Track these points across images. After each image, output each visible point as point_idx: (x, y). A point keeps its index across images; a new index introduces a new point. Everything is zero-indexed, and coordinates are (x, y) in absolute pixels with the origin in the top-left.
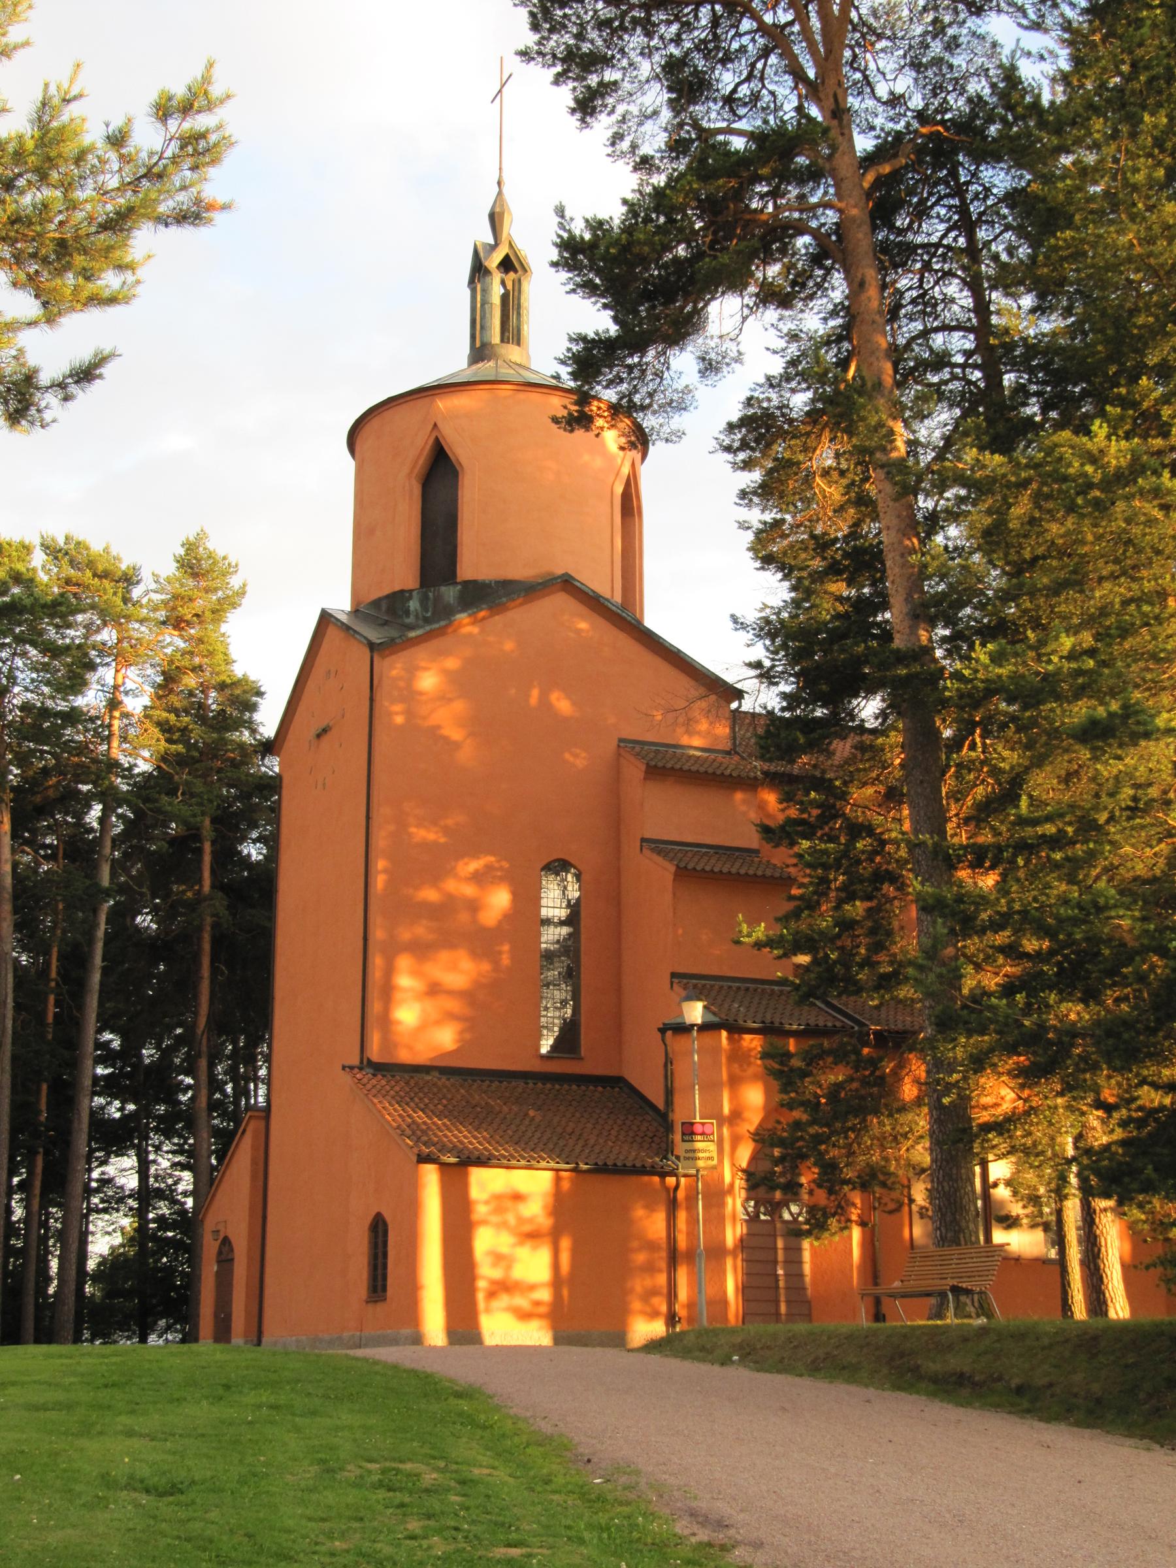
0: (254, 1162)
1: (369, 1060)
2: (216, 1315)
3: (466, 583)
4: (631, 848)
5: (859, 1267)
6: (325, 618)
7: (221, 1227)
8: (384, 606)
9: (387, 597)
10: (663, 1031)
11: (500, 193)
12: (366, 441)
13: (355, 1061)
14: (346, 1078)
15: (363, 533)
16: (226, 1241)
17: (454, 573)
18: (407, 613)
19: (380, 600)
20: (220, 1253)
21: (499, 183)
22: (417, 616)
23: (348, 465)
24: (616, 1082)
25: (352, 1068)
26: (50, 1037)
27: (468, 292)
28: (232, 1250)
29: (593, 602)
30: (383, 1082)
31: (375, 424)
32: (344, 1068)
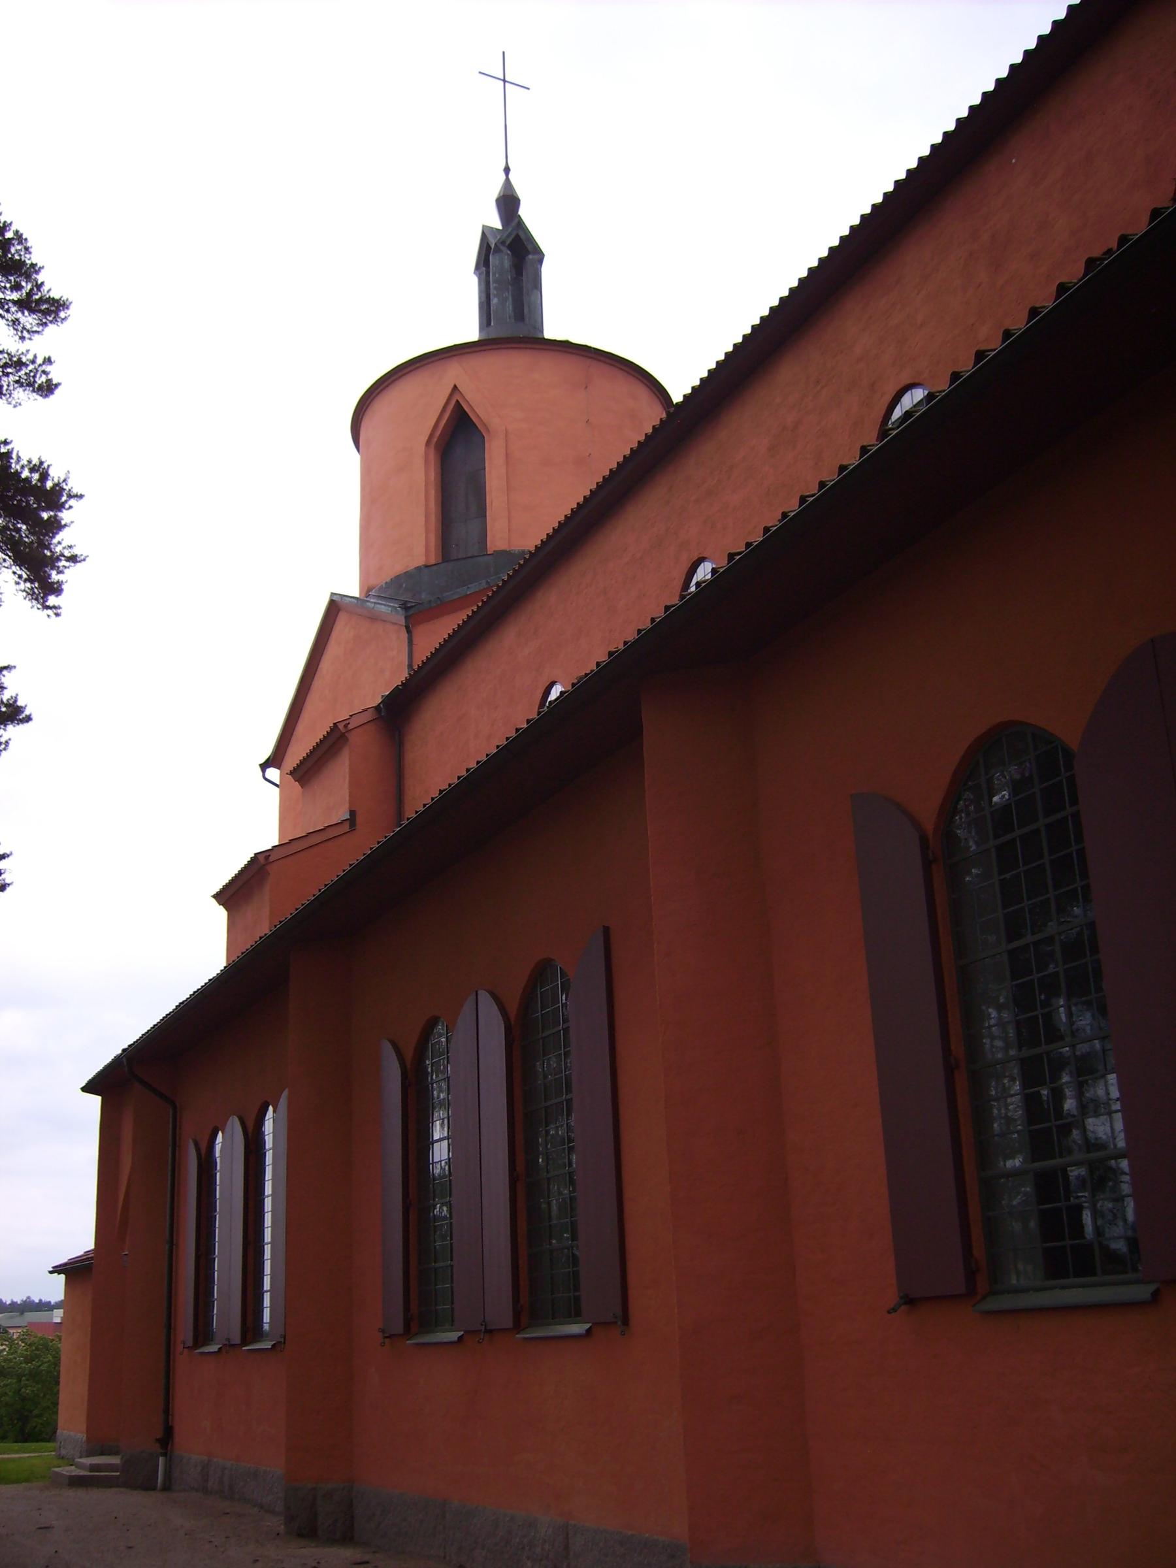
21: (507, 170)
27: (474, 281)
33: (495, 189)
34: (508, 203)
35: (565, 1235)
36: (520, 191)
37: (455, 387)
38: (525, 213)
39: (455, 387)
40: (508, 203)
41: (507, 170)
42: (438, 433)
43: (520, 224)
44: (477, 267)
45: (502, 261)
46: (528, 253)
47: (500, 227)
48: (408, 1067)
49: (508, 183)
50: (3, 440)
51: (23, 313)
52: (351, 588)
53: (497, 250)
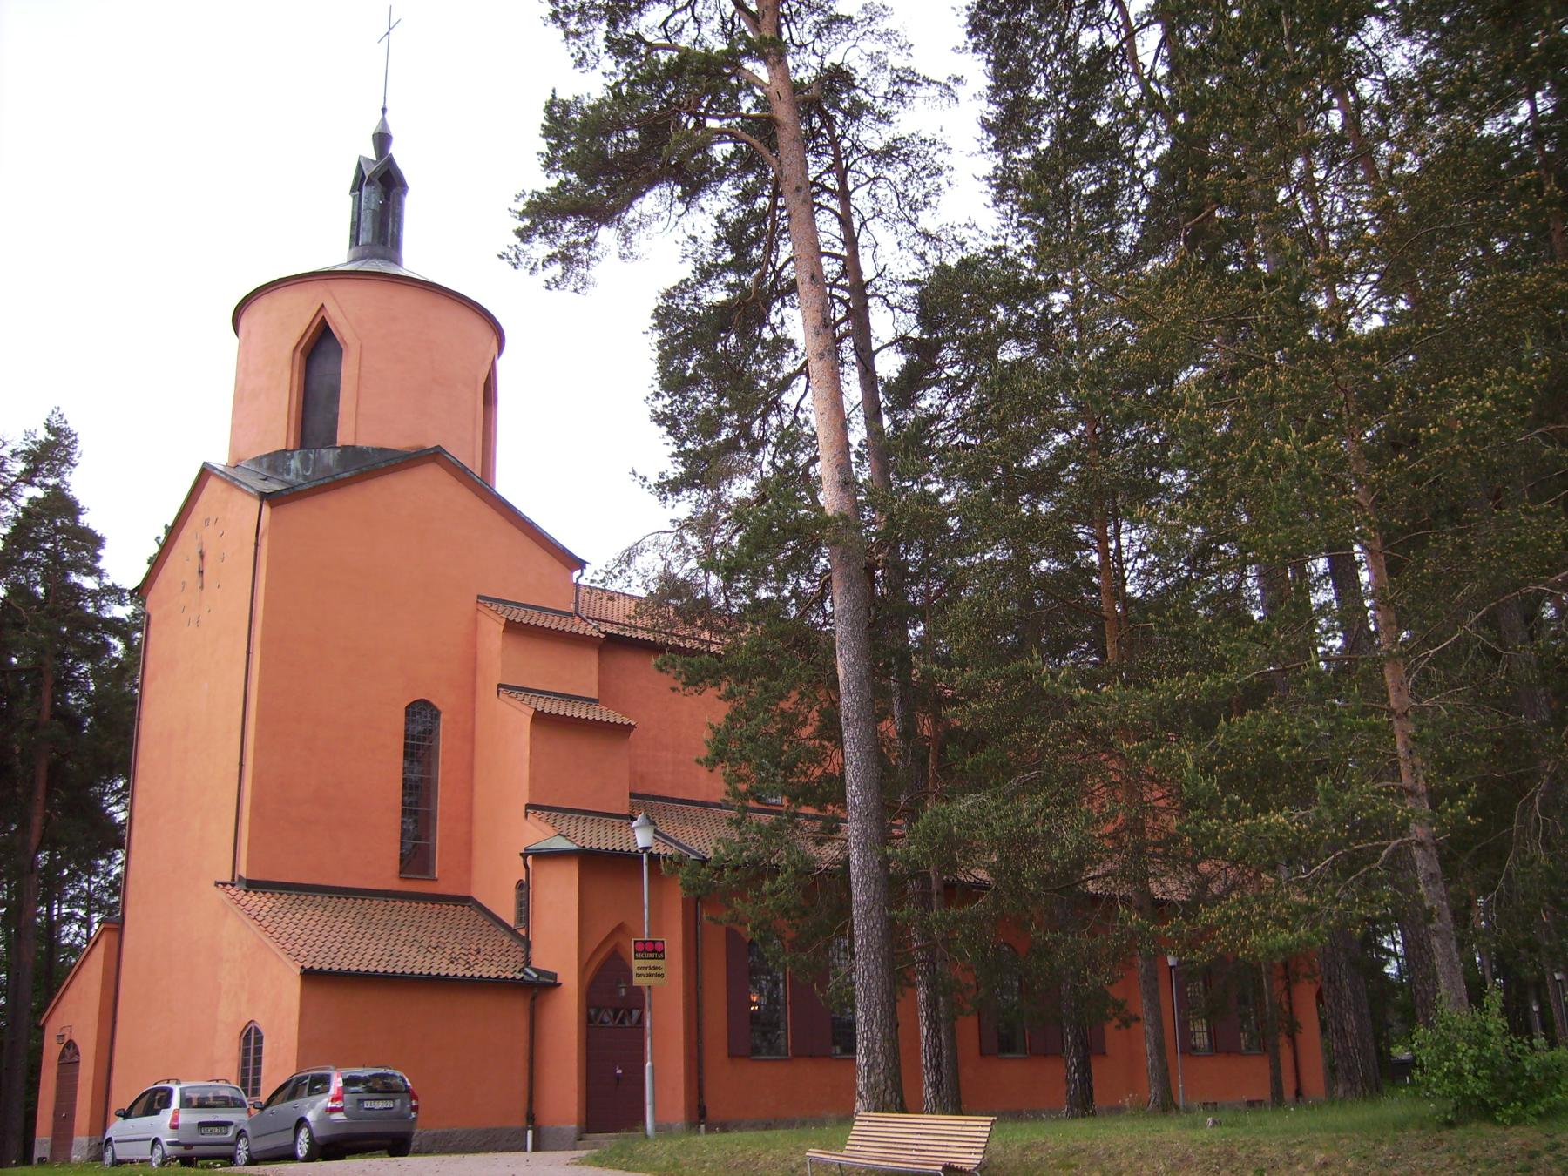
0: (105, 971)
1: (240, 876)
2: (56, 1114)
3: (345, 448)
4: (487, 691)
5: (1008, 1111)
6: (206, 473)
7: (66, 1032)
8: (265, 462)
9: (269, 455)
10: (524, 855)
11: (384, 119)
12: (247, 321)
13: (228, 879)
14: (221, 894)
15: (241, 398)
16: (71, 1044)
17: (335, 441)
18: (288, 471)
19: (262, 457)
20: (62, 1055)
21: (384, 110)
22: (297, 475)
23: (234, 341)
24: (465, 900)
25: (224, 884)
26: (1356, 548)
27: (349, 200)
28: (77, 1053)
29: (460, 472)
30: (273, 900)
31: (264, 302)
32: (217, 884)
33: (373, 126)
34: (382, 140)
35: (1081, 427)
36: (394, 130)
37: (323, 306)
38: (395, 150)
39: (323, 306)
40: (382, 140)
41: (384, 110)
42: (312, 330)
43: (391, 161)
44: (352, 190)
45: (371, 195)
46: (395, 186)
47: (374, 158)
48: (562, 844)
49: (383, 122)
50: (521, 859)
51: (1188, 896)
52: (220, 458)
53: (370, 182)
